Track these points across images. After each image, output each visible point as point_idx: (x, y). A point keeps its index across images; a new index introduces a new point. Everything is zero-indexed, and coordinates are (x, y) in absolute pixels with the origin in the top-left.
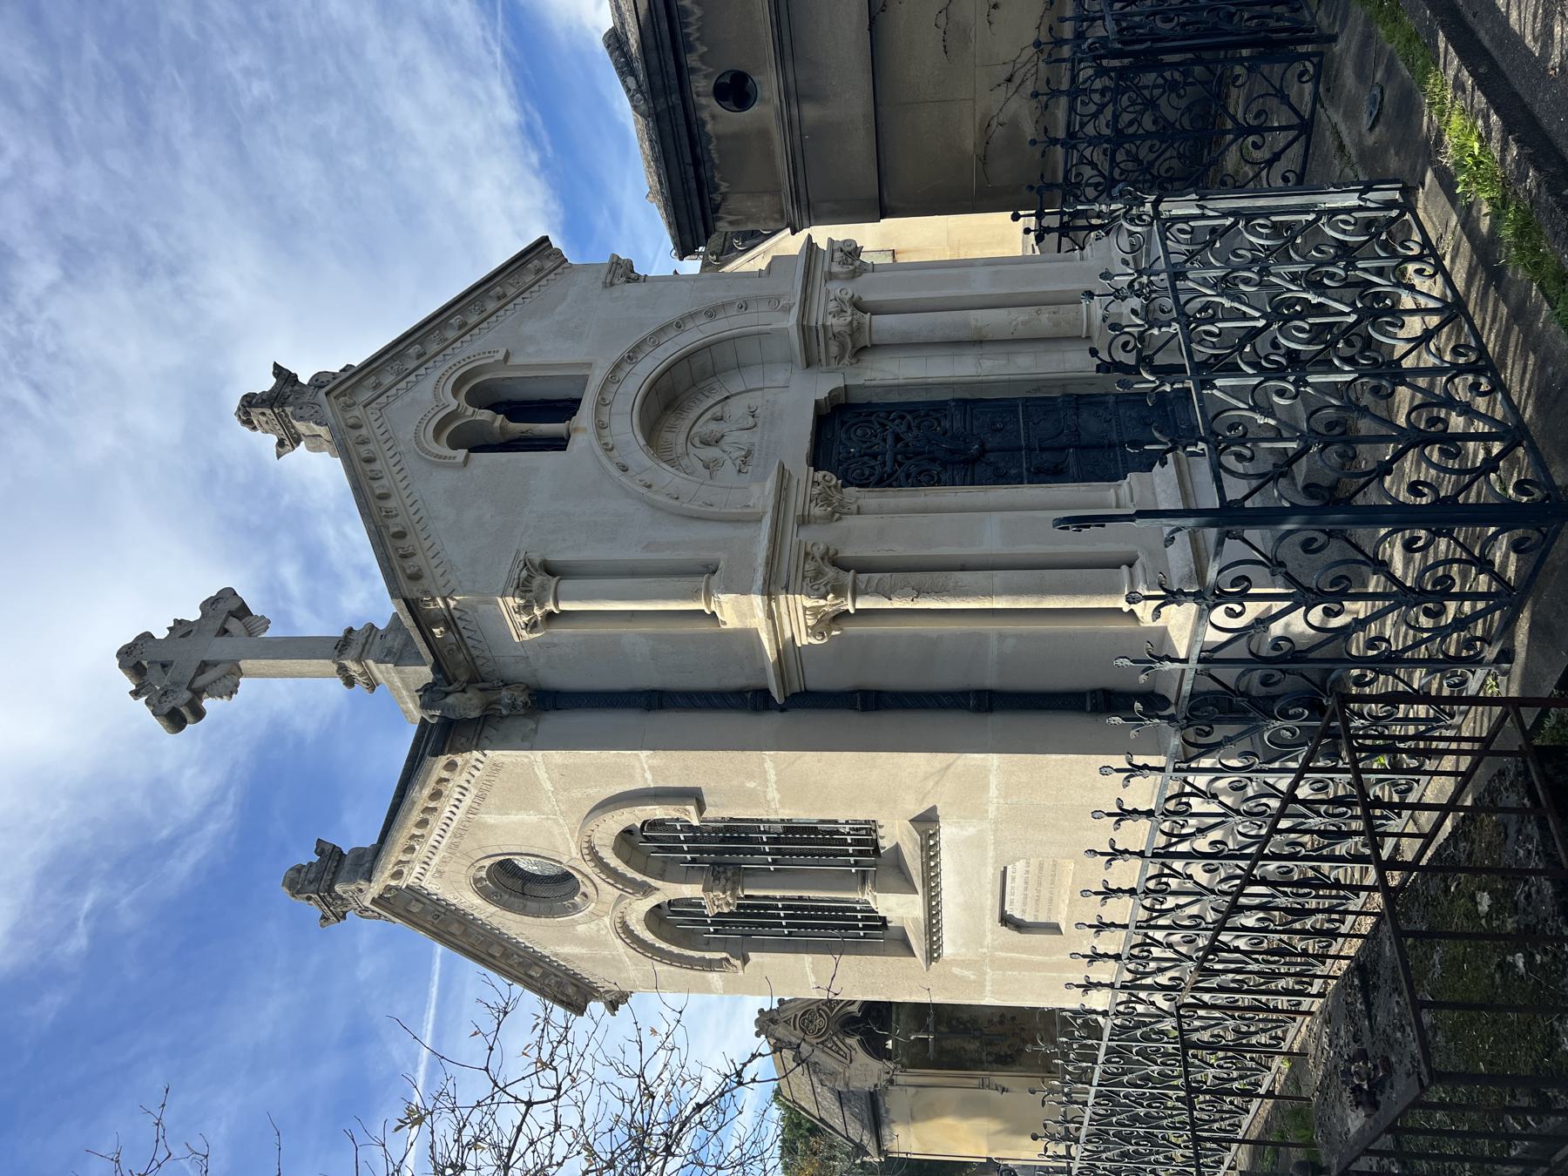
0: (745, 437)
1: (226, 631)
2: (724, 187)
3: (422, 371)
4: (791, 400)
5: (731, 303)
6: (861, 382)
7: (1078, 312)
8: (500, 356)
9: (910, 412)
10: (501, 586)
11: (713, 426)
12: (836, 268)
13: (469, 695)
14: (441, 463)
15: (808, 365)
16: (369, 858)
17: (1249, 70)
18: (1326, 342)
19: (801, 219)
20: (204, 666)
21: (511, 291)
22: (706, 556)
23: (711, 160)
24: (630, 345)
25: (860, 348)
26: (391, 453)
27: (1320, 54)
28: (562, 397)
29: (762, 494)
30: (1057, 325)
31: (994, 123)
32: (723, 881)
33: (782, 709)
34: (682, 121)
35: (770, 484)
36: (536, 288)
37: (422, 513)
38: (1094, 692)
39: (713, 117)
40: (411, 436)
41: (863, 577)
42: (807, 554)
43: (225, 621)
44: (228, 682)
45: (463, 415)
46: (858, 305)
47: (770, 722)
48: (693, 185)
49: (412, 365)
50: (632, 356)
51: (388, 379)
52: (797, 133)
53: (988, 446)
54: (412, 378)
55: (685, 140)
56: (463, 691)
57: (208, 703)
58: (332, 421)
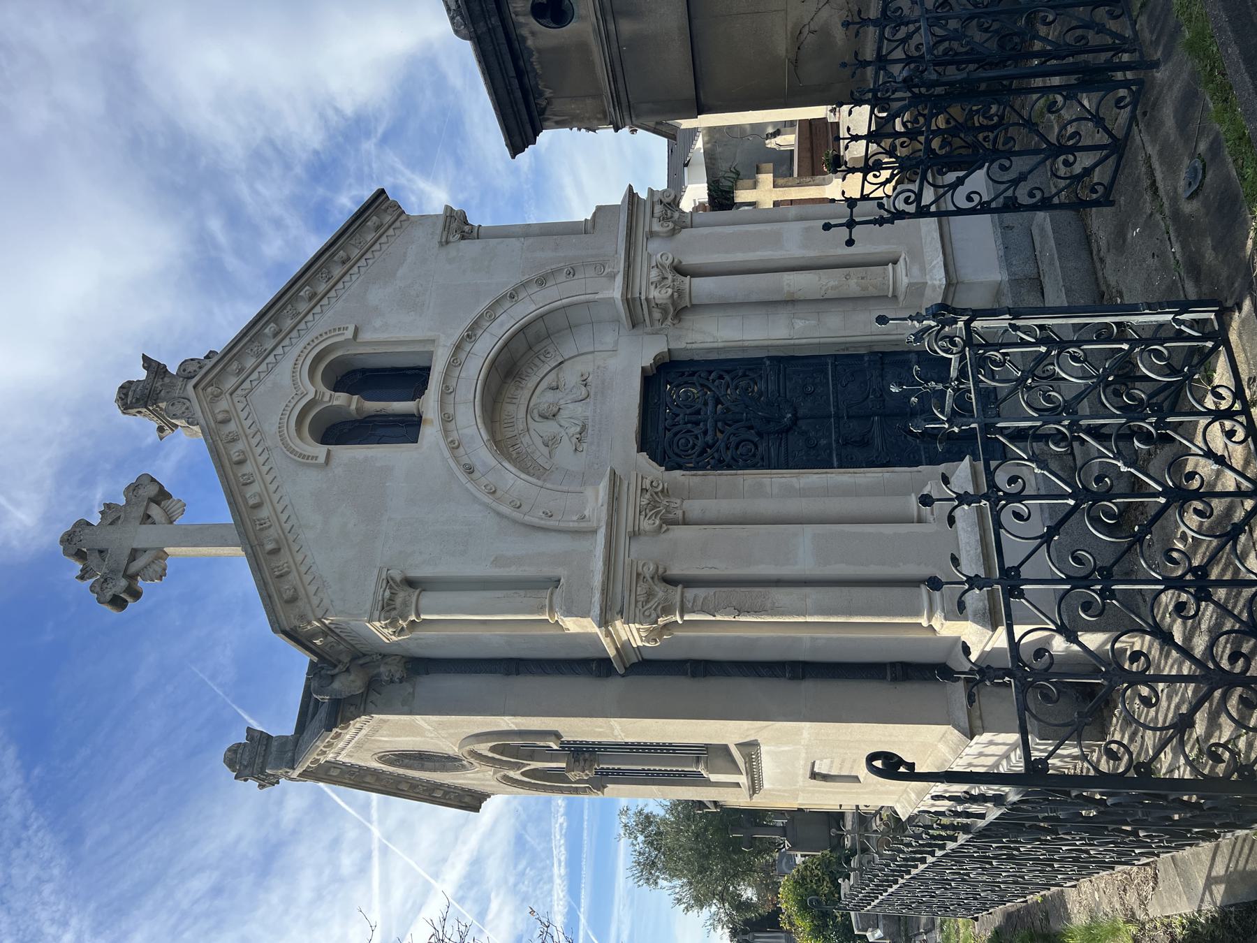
0: (579, 409)
1: (149, 517)
2: (548, 93)
3: (279, 350)
4: (623, 361)
5: (560, 270)
6: (683, 345)
7: (885, 276)
8: (349, 334)
9: (728, 372)
10: (368, 606)
11: (550, 396)
12: (657, 227)
13: (352, 677)
14: (307, 461)
15: (634, 327)
16: (290, 747)
17: (1065, 98)
18: (1134, 535)
19: (623, 118)
20: (134, 554)
21: (355, 253)
22: (548, 571)
23: (534, 70)
24: (468, 322)
25: (680, 310)
26: (259, 450)
27: (1140, 82)
28: (411, 365)
29: (596, 500)
30: (864, 289)
31: (806, 30)
32: (582, 763)
33: (623, 676)
34: (503, 40)
35: (603, 487)
36: (377, 247)
37: (293, 521)
38: (893, 664)
39: (533, 33)
40: (275, 428)
41: (691, 593)
42: (638, 575)
43: (147, 507)
44: (157, 567)
45: (322, 401)
46: (679, 270)
47: (612, 688)
48: (519, 94)
49: (269, 345)
50: (471, 335)
51: (250, 362)
52: (614, 46)
53: (801, 412)
54: (271, 359)
55: (508, 57)
56: (348, 670)
57: (141, 583)
58: (202, 421)
